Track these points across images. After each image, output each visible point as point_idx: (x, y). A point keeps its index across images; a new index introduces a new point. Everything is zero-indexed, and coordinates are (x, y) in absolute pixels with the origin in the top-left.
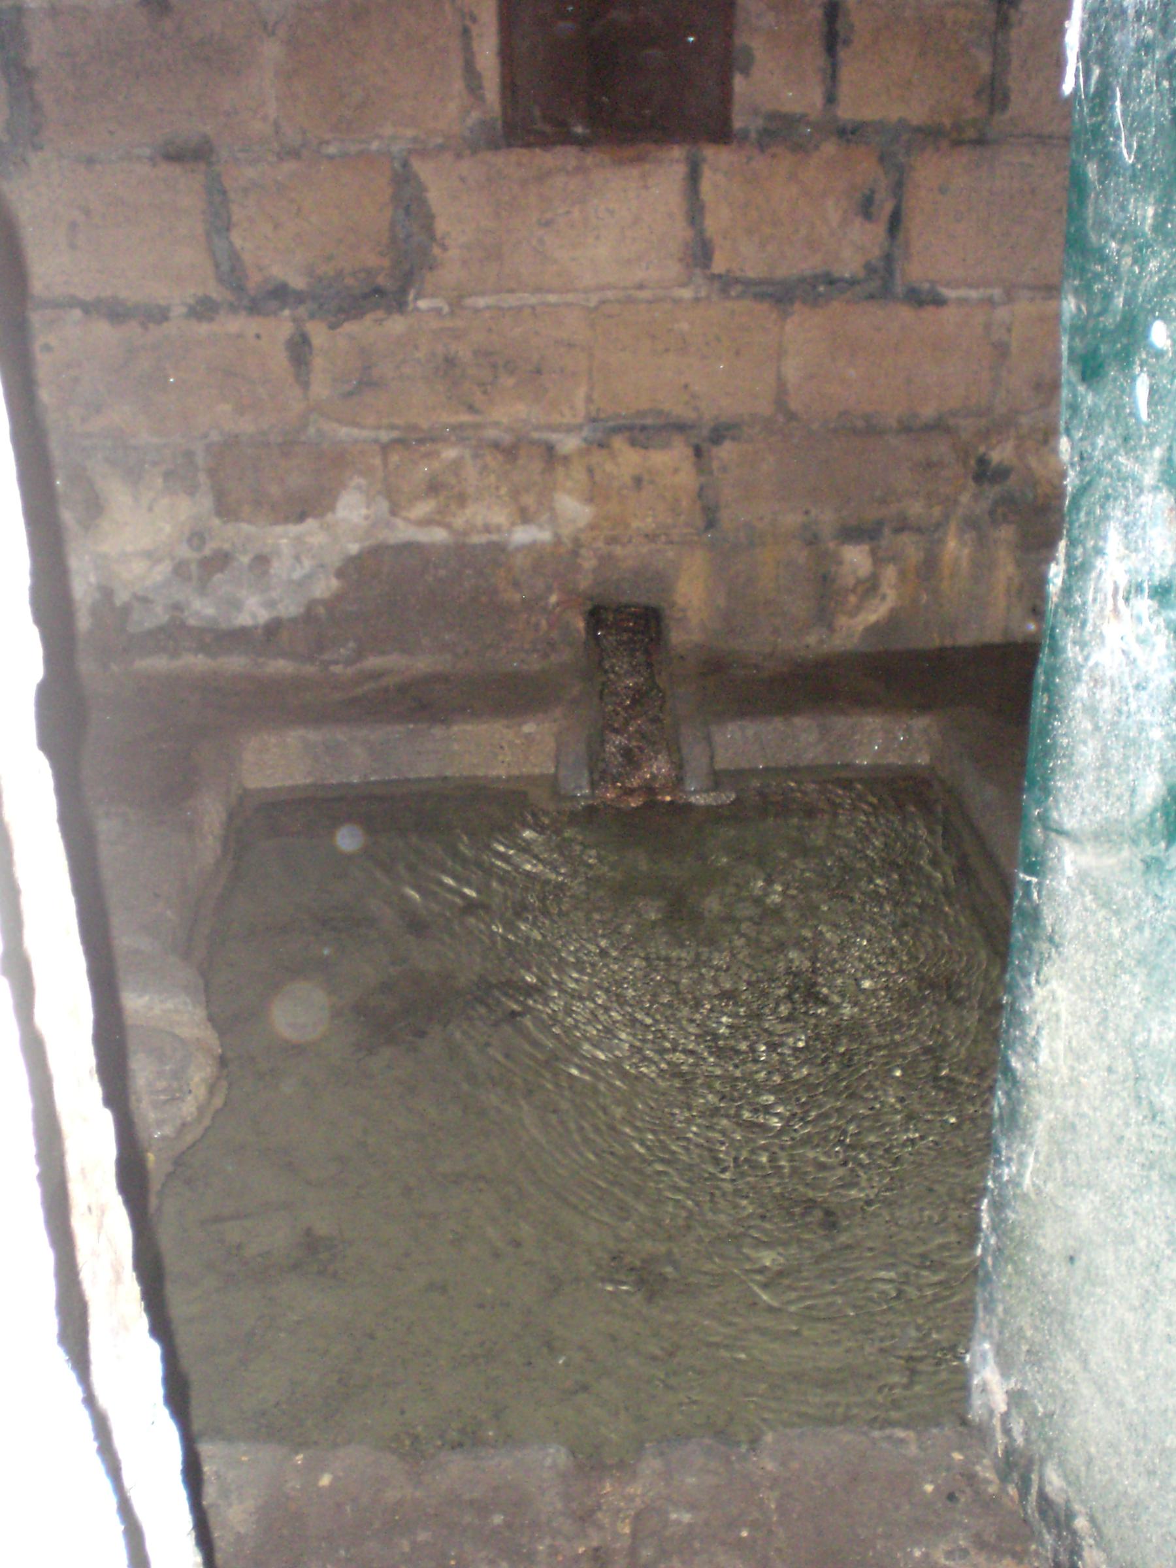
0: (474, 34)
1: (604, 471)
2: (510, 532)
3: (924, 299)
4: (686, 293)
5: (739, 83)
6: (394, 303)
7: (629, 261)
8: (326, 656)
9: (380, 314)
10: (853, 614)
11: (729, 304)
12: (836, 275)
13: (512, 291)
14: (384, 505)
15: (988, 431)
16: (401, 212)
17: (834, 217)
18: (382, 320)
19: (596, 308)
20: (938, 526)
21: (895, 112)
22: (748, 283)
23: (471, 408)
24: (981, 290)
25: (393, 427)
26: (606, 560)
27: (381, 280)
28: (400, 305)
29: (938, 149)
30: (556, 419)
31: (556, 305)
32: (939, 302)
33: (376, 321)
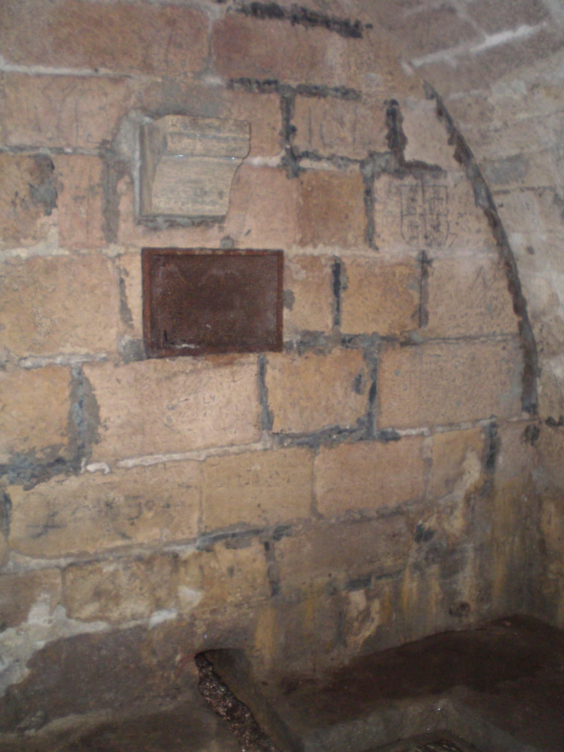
0: (127, 283)
1: (210, 567)
2: (149, 617)
3: (389, 437)
4: (259, 446)
5: (286, 312)
6: (71, 469)
7: (224, 429)
8: (22, 725)
9: (62, 477)
10: (356, 635)
11: (282, 451)
12: (342, 428)
13: (151, 454)
14: (62, 611)
15: (423, 512)
16: (77, 405)
17: (340, 392)
18: (63, 481)
19: (204, 461)
20: (399, 572)
21: (372, 328)
22: (293, 436)
23: (124, 536)
24: (417, 430)
25: (69, 555)
26: (211, 626)
27: (62, 453)
28: (76, 470)
29: (394, 349)
30: (180, 536)
31: (179, 461)
32: (397, 438)
33: (58, 482)
